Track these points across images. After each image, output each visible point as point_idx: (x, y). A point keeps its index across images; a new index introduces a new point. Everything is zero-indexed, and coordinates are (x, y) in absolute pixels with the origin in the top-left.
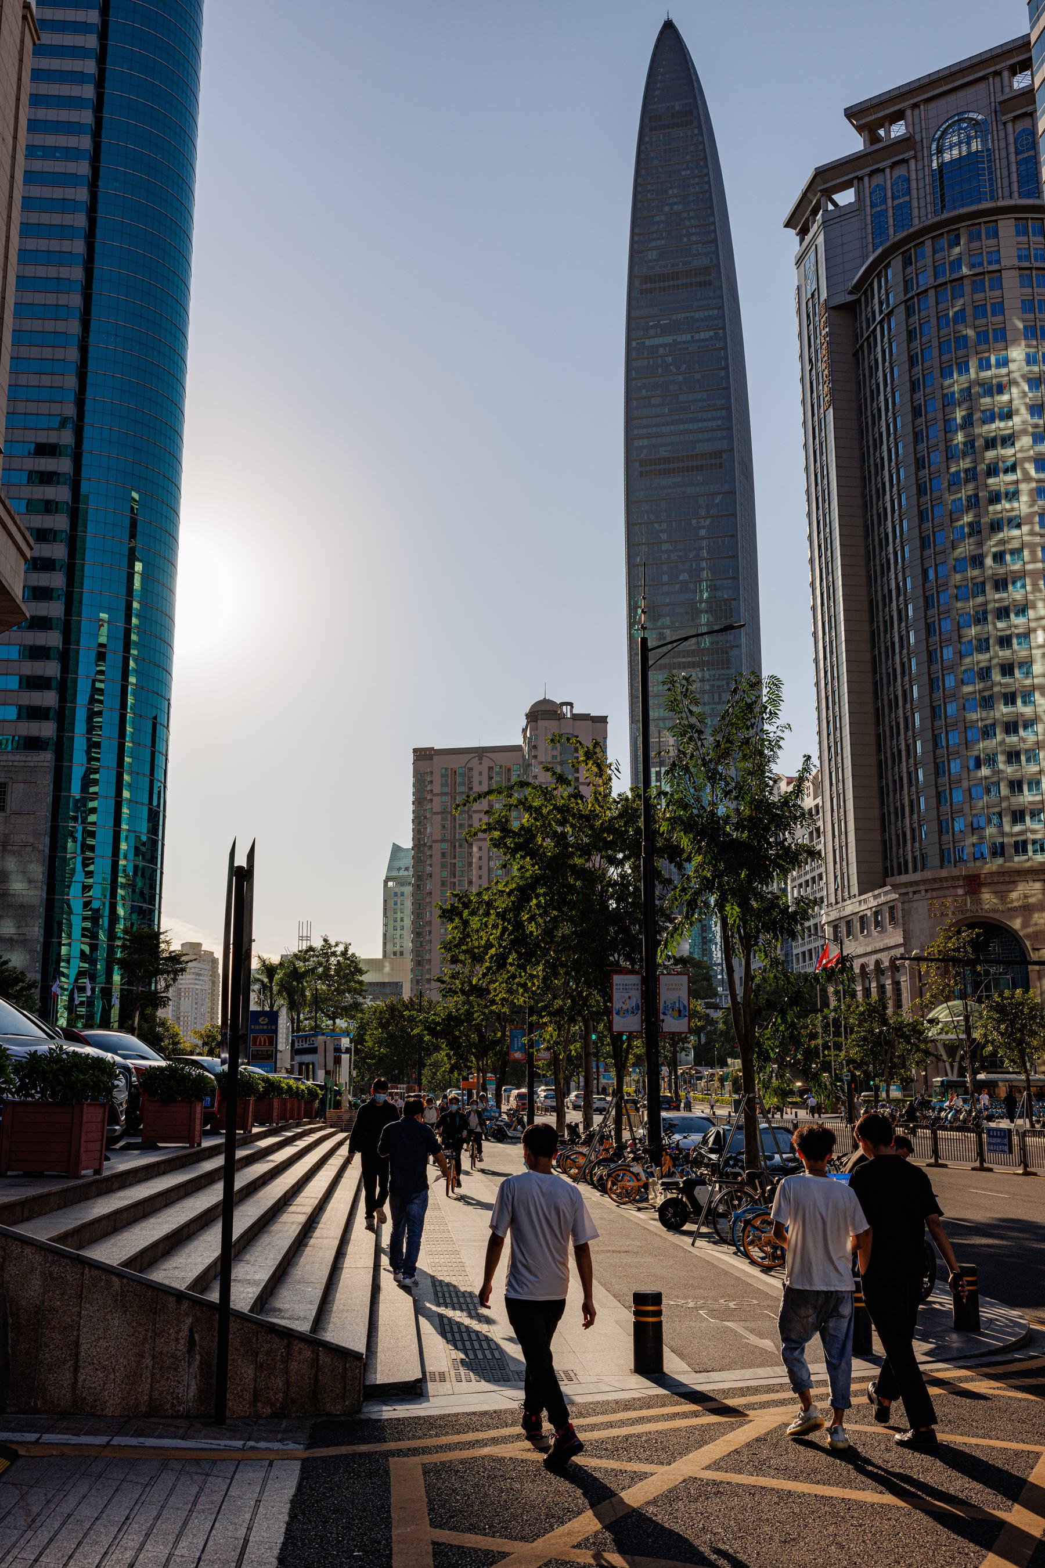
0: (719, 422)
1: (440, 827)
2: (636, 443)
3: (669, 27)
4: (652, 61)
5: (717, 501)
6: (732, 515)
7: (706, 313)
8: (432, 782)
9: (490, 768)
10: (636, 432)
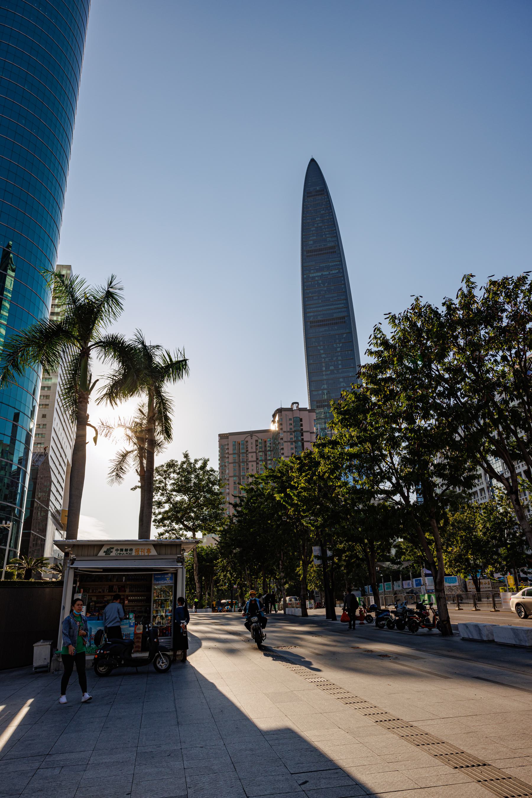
0: (343, 305)
2: (308, 315)
3: (313, 161)
4: (307, 173)
5: (344, 336)
6: (351, 342)
7: (335, 263)
8: (228, 449)
9: (257, 441)
10: (308, 310)
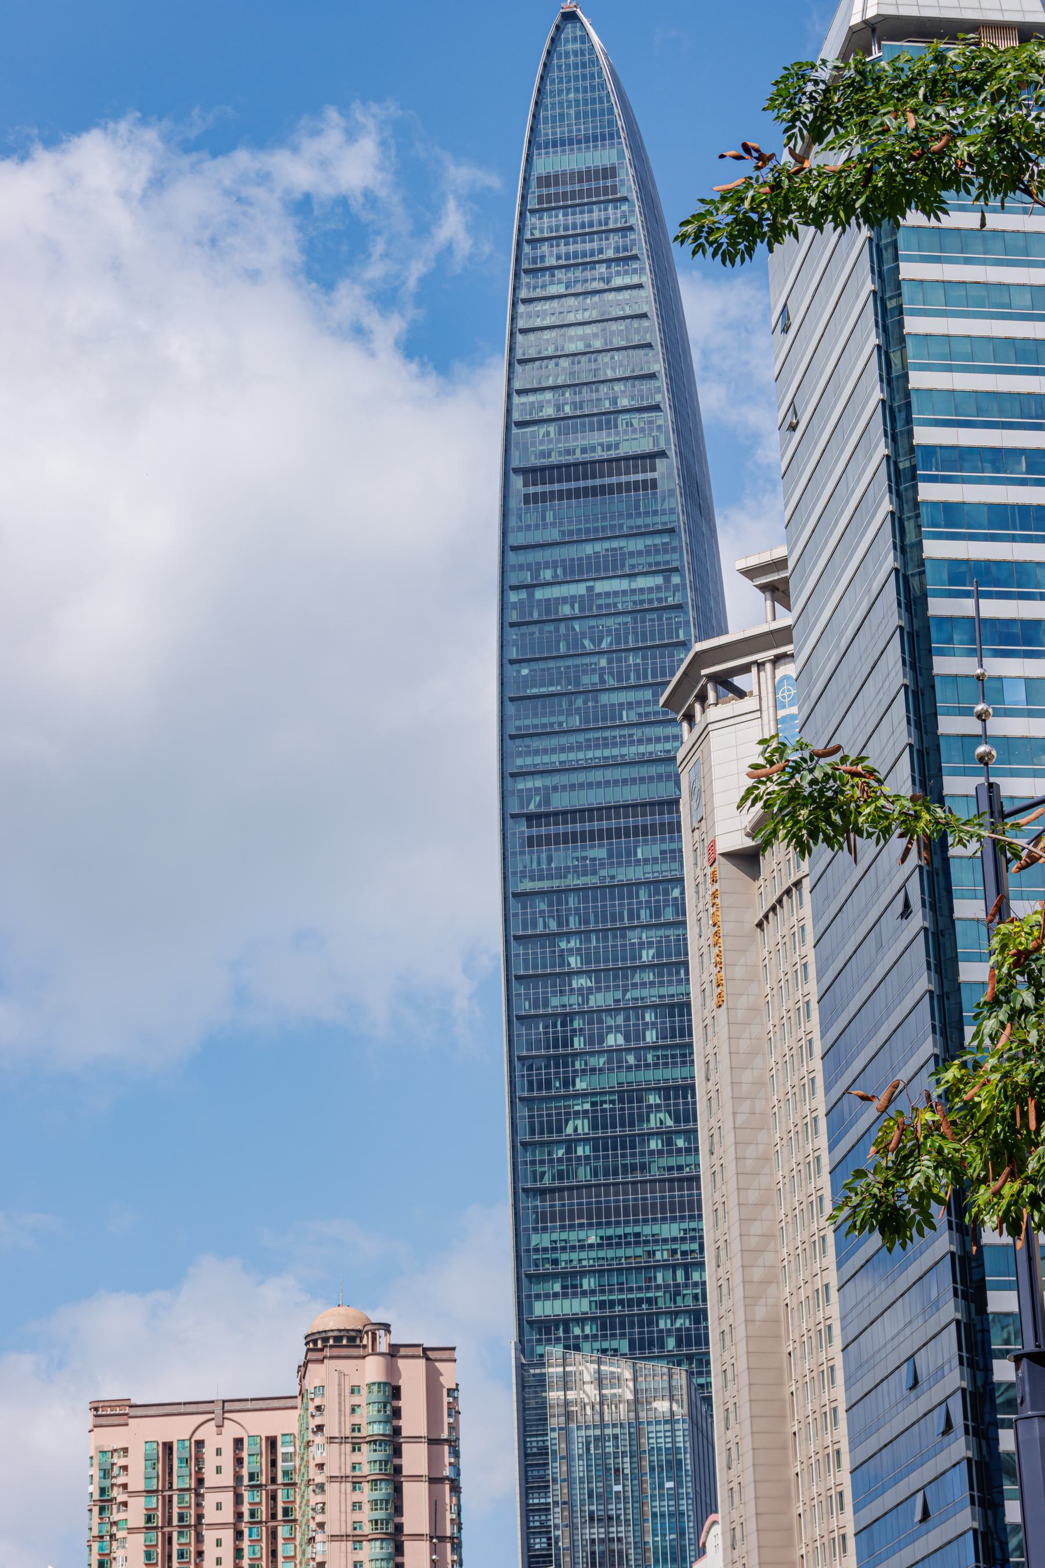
1: (142, 1556)
9: (238, 1443)
10: (519, 762)
